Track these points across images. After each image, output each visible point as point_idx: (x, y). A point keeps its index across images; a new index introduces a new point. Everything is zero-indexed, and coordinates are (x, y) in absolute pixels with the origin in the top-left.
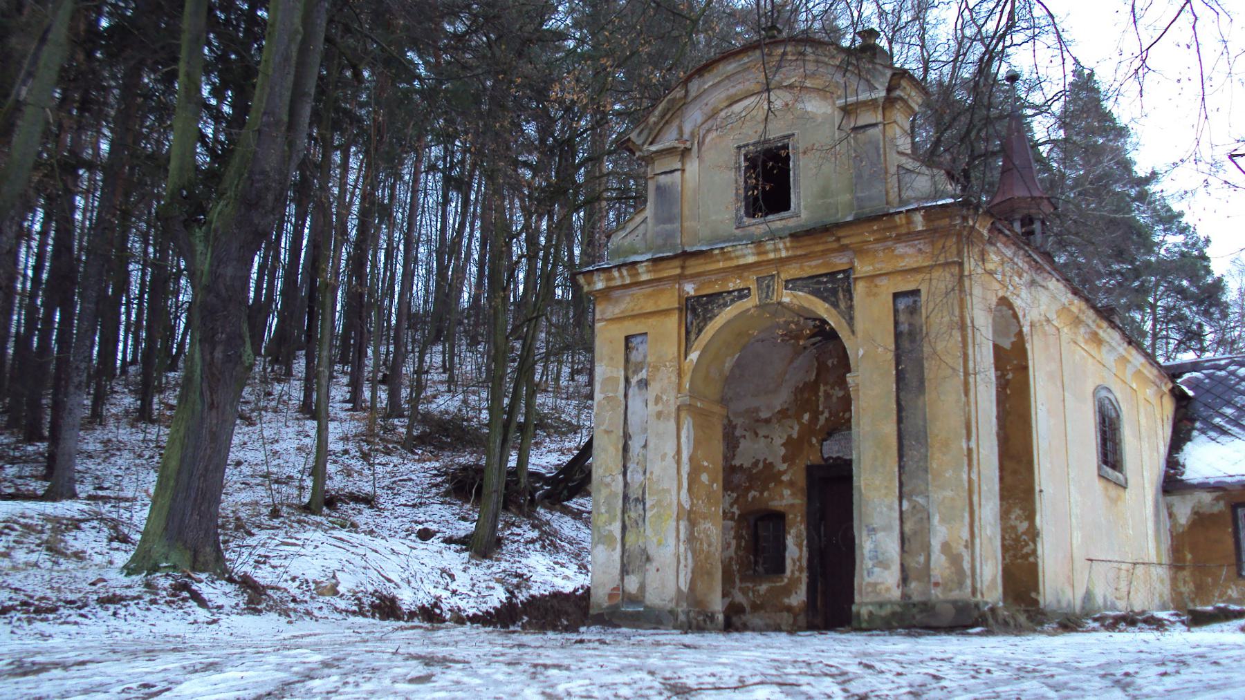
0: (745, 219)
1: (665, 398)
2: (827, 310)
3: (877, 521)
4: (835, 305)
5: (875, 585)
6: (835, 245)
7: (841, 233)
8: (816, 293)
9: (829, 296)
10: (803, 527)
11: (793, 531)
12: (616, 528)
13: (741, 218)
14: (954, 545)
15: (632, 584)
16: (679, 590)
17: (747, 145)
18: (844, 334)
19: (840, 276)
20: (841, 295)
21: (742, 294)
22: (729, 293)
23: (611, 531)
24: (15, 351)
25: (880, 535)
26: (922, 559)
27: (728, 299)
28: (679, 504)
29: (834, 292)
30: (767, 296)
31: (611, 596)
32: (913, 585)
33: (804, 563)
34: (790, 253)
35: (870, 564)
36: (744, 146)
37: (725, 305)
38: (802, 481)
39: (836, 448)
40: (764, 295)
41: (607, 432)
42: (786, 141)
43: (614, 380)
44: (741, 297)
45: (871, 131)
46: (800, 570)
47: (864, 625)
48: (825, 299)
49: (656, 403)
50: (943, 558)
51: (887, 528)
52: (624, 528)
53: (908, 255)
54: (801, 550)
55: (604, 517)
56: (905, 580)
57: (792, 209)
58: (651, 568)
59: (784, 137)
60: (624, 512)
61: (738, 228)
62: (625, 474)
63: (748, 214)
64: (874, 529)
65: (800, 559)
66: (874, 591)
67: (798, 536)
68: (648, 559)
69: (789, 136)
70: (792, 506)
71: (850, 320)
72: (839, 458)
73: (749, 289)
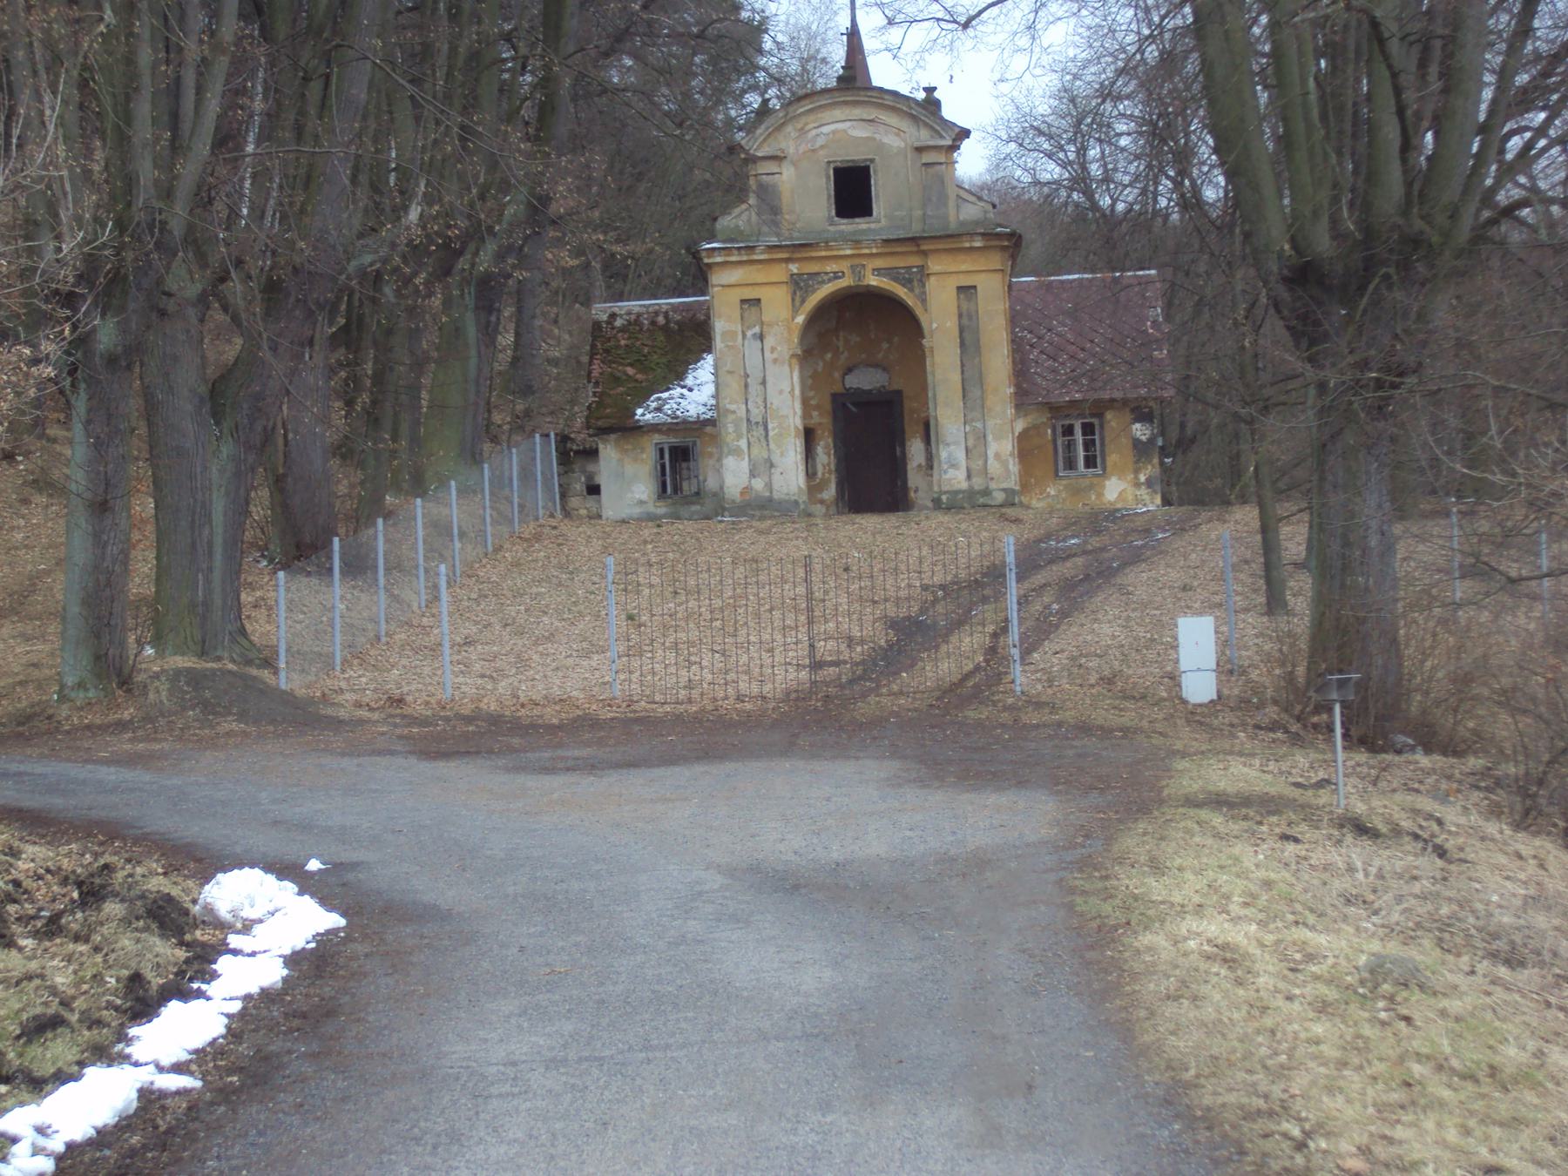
3: (949, 439)
4: (911, 290)
5: (950, 480)
6: (915, 249)
8: (895, 279)
9: (907, 282)
11: (822, 443)
12: (743, 443)
15: (758, 484)
16: (799, 487)
18: (919, 311)
20: (916, 283)
21: (837, 276)
22: (827, 273)
23: (738, 446)
25: (952, 447)
26: (980, 463)
27: (826, 278)
28: (796, 427)
29: (910, 281)
31: (742, 494)
32: (974, 480)
33: (833, 467)
34: (880, 251)
35: (945, 467)
37: (823, 282)
38: (828, 406)
41: (730, 372)
43: (734, 333)
44: (837, 278)
45: (938, 168)
46: (830, 472)
48: (904, 285)
51: (956, 443)
52: (749, 444)
53: (964, 264)
56: (969, 477)
57: (875, 213)
58: (776, 472)
59: (866, 160)
65: (829, 464)
67: (826, 447)
68: (772, 465)
69: (872, 161)
70: (820, 424)
71: (924, 301)
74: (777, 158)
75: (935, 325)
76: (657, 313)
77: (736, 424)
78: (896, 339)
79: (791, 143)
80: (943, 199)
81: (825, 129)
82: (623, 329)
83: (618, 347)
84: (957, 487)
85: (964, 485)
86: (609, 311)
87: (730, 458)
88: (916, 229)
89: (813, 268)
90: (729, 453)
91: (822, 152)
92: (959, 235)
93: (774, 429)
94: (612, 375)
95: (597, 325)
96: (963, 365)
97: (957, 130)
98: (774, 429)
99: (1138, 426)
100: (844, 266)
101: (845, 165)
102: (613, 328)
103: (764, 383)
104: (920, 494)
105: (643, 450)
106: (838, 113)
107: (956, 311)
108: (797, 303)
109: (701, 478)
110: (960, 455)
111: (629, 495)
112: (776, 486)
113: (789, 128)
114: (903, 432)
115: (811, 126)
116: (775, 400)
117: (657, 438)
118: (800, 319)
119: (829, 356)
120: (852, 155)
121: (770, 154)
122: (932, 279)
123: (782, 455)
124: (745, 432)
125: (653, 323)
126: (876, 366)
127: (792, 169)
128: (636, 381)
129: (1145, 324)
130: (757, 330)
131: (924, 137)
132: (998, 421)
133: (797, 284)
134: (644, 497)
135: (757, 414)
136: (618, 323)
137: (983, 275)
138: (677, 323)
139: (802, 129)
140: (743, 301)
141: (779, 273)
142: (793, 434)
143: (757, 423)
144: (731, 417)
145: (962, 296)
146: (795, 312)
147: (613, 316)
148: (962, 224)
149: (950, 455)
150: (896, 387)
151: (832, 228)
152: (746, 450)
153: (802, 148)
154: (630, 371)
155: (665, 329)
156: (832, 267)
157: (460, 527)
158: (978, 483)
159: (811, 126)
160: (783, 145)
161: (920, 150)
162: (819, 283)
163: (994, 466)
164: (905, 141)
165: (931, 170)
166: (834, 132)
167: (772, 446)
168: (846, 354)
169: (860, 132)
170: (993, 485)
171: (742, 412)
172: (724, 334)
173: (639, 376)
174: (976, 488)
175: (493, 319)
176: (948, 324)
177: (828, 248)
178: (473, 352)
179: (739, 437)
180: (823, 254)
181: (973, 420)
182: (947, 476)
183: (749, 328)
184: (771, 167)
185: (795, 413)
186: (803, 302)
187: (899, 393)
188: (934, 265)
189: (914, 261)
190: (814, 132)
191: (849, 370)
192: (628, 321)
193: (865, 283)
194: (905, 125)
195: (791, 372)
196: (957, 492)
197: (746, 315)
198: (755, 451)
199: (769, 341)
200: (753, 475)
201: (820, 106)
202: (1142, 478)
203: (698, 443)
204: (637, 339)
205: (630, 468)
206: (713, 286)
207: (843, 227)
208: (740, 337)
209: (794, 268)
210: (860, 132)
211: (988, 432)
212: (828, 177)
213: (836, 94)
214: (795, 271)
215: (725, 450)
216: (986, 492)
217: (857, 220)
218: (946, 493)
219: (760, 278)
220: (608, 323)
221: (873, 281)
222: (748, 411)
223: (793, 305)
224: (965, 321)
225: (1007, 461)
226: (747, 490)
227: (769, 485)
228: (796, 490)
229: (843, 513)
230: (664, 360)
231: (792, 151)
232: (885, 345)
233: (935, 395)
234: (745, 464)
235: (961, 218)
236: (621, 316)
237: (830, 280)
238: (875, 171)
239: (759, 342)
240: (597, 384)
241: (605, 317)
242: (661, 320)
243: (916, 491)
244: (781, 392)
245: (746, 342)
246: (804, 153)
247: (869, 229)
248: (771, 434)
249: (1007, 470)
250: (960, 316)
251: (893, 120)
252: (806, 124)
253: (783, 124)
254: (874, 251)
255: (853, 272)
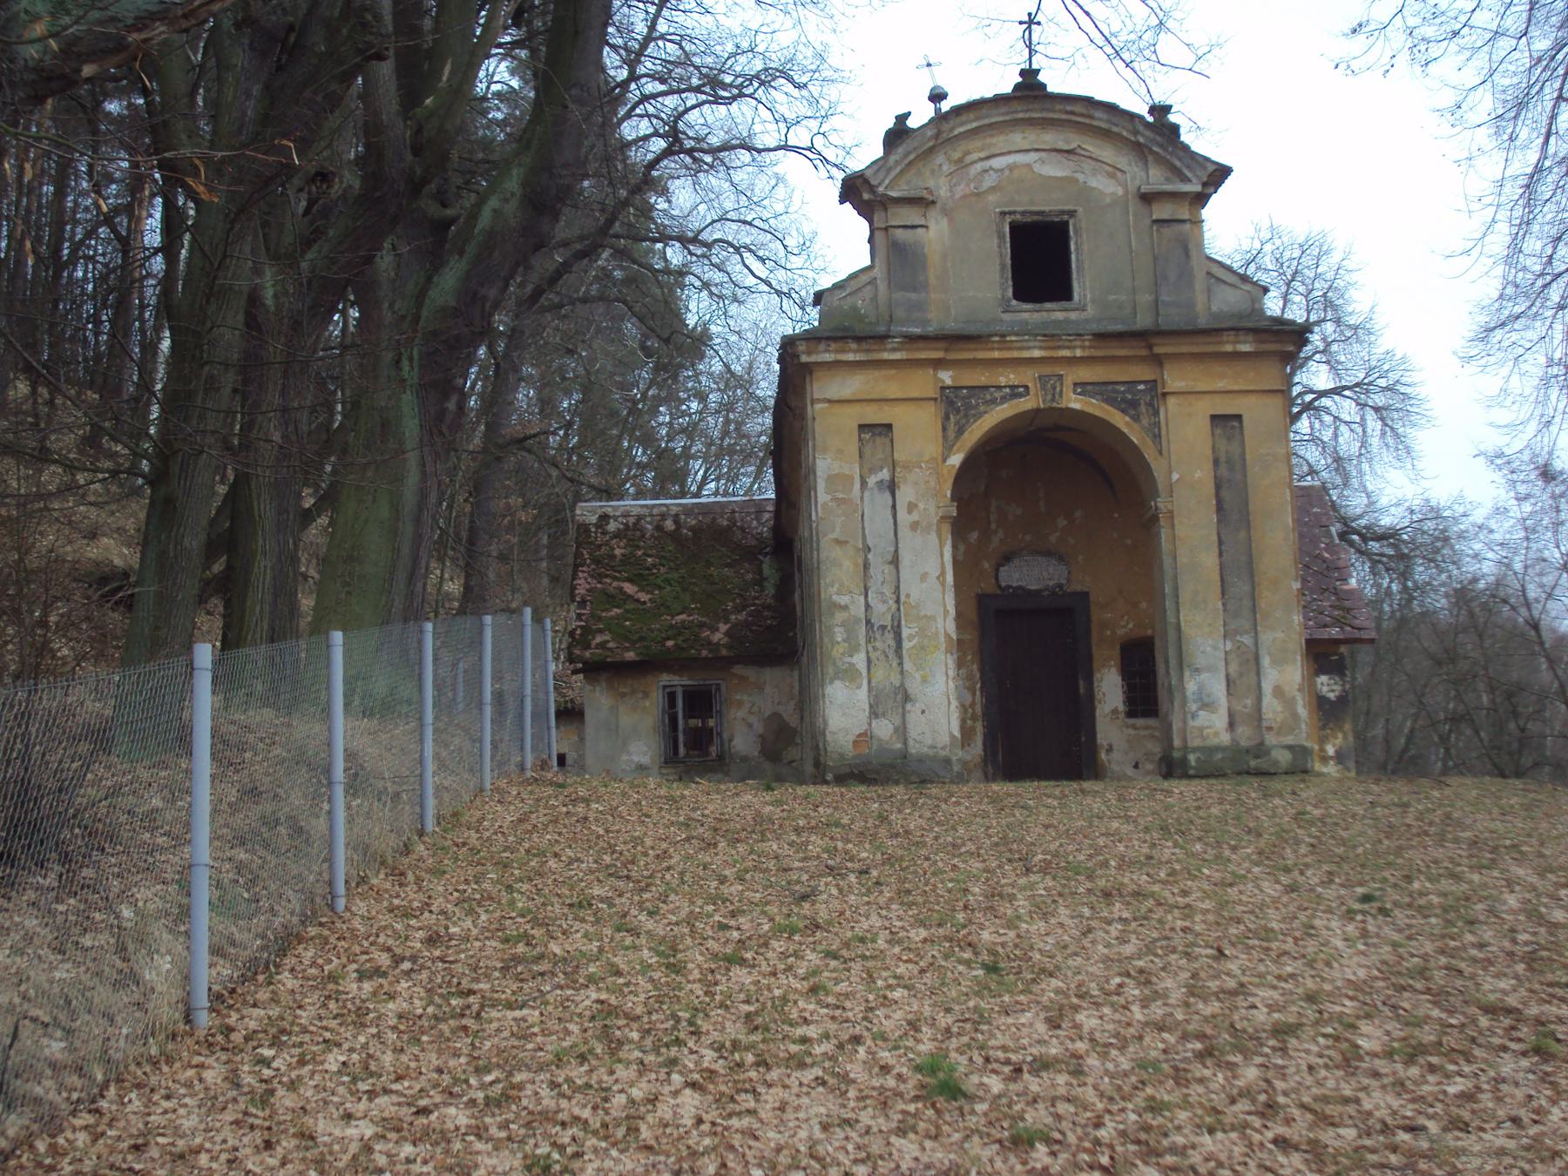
0: (1014, 302)
1: (921, 506)
2: (1127, 424)
3: (1201, 661)
4: (1136, 418)
5: (1201, 729)
6: (1144, 352)
7: (1156, 340)
8: (1110, 401)
9: (1129, 407)
10: (975, 667)
12: (859, 660)
13: (1009, 301)
14: (1286, 688)
15: (884, 729)
16: (952, 736)
17: (1014, 213)
18: (1149, 453)
19: (1141, 387)
20: (1143, 408)
21: (1015, 392)
22: (999, 388)
24: (173, 347)
25: (1204, 676)
27: (998, 395)
28: (947, 635)
29: (1134, 404)
30: (1053, 400)
32: (1240, 730)
33: (978, 709)
34: (1087, 353)
35: (1194, 707)
36: (1010, 213)
37: (993, 401)
39: (1017, 575)
40: (1049, 397)
42: (1065, 217)
43: (847, 480)
44: (1014, 396)
45: (1177, 227)
47: (1191, 772)
49: (910, 512)
50: (1275, 702)
51: (1211, 669)
52: (869, 661)
54: (974, 694)
55: (841, 649)
56: (1231, 725)
57: (1076, 296)
58: (914, 710)
59: (1063, 212)
60: (868, 641)
61: (1005, 312)
62: (866, 596)
63: (1017, 296)
64: (1197, 670)
65: (973, 705)
66: (1202, 736)
68: (907, 698)
69: (1072, 213)
71: (1157, 437)
72: (1020, 587)
73: (1026, 387)
74: (922, 202)
75: (1175, 476)
76: (663, 516)
77: (849, 627)
78: (1078, 514)
79: (943, 181)
80: (1186, 275)
81: (997, 163)
82: (617, 535)
83: (613, 557)
84: (1214, 741)
85: (1225, 738)
86: (600, 512)
87: (838, 684)
88: (1143, 321)
89: (980, 378)
90: (836, 677)
91: (991, 198)
92: (1218, 331)
93: (911, 638)
94: (603, 591)
95: (583, 529)
96: (1220, 542)
97: (1211, 168)
98: (911, 638)
99: (1323, 679)
100: (1028, 376)
101: (1029, 219)
102: (604, 533)
103: (895, 561)
104: (1115, 755)
105: (646, 695)
106: (1018, 138)
107: (1209, 452)
108: (951, 434)
109: (725, 736)
110: (1218, 689)
111: (625, 757)
112: (913, 732)
113: (940, 159)
114: (1089, 658)
115: (975, 156)
116: (913, 589)
117: (666, 679)
118: (956, 460)
119: (974, 536)
120: (1047, 204)
121: (912, 194)
122: (1171, 401)
123: (924, 681)
124: (863, 642)
125: (659, 528)
126: (1048, 554)
127: (944, 222)
128: (638, 601)
129: (1318, 547)
130: (885, 474)
131: (1156, 179)
132: (1280, 635)
133: (951, 403)
134: (646, 760)
135: (882, 612)
136: (612, 526)
137: (1252, 400)
138: (691, 529)
139: (960, 160)
140: (863, 427)
141: (922, 383)
142: (943, 647)
143: (883, 628)
144: (840, 617)
145: (1218, 431)
146: (948, 449)
147: (604, 518)
148: (1215, 316)
149: (1201, 688)
150: (1078, 588)
151: (1007, 317)
152: (864, 672)
153: (960, 190)
154: (629, 588)
155: (675, 536)
156: (1008, 378)
157: (350, 756)
158: (1245, 735)
159: (975, 156)
160: (931, 183)
161: (1147, 198)
162: (986, 403)
163: (1272, 708)
164: (1124, 185)
165: (1167, 231)
166: (1011, 168)
167: (908, 666)
168: (1001, 533)
169: (1054, 169)
170: (1271, 739)
171: (858, 610)
172: (831, 479)
173: (644, 597)
174: (1244, 743)
175: (451, 405)
176: (1198, 474)
177: (1004, 345)
178: (412, 459)
179: (853, 650)
180: (996, 354)
181: (1236, 632)
182: (1198, 723)
183: (872, 471)
184: (911, 215)
185: (946, 612)
186: (960, 431)
187: (1084, 596)
188: (1175, 379)
189: (1143, 372)
190: (979, 166)
191: (1007, 559)
192: (626, 525)
193: (1063, 405)
194: (1123, 160)
195: (941, 546)
196: (1217, 748)
197: (867, 450)
198: (879, 674)
199: (905, 494)
200: (874, 713)
201: (990, 125)
202: (1331, 750)
203: (723, 688)
204: (639, 548)
205: (626, 719)
206: (813, 402)
207: (1025, 316)
208: (857, 485)
209: (946, 377)
210: (1054, 169)
211: (1263, 652)
212: (1001, 237)
213: (1016, 106)
214: (949, 382)
215: (831, 670)
216: (1260, 750)
217: (1048, 305)
218: (1195, 750)
219: (893, 390)
220: (597, 526)
221: (1074, 402)
222: (867, 606)
223: (945, 437)
224: (1224, 471)
225: (1294, 699)
226: (865, 737)
227: (902, 731)
228: (946, 740)
229: (994, 780)
230: (675, 575)
231: (943, 192)
232: (1062, 522)
233: (1176, 589)
234: (862, 694)
235: (1214, 308)
236: (616, 518)
237: (1004, 399)
238: (1076, 232)
239: (887, 496)
240: (583, 603)
241: (594, 519)
242: (669, 525)
243: (1110, 749)
244: (924, 577)
245: (866, 494)
246: (965, 197)
247: (1067, 321)
248: (906, 645)
249: (1295, 716)
250: (1216, 462)
251: (1107, 153)
252: (968, 153)
253: (931, 150)
254: (1078, 353)
255: (1043, 388)
